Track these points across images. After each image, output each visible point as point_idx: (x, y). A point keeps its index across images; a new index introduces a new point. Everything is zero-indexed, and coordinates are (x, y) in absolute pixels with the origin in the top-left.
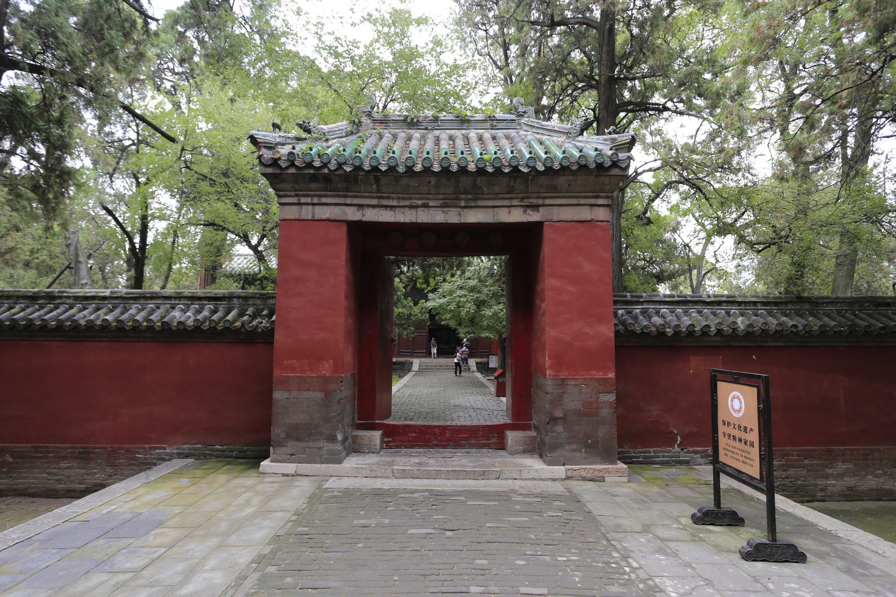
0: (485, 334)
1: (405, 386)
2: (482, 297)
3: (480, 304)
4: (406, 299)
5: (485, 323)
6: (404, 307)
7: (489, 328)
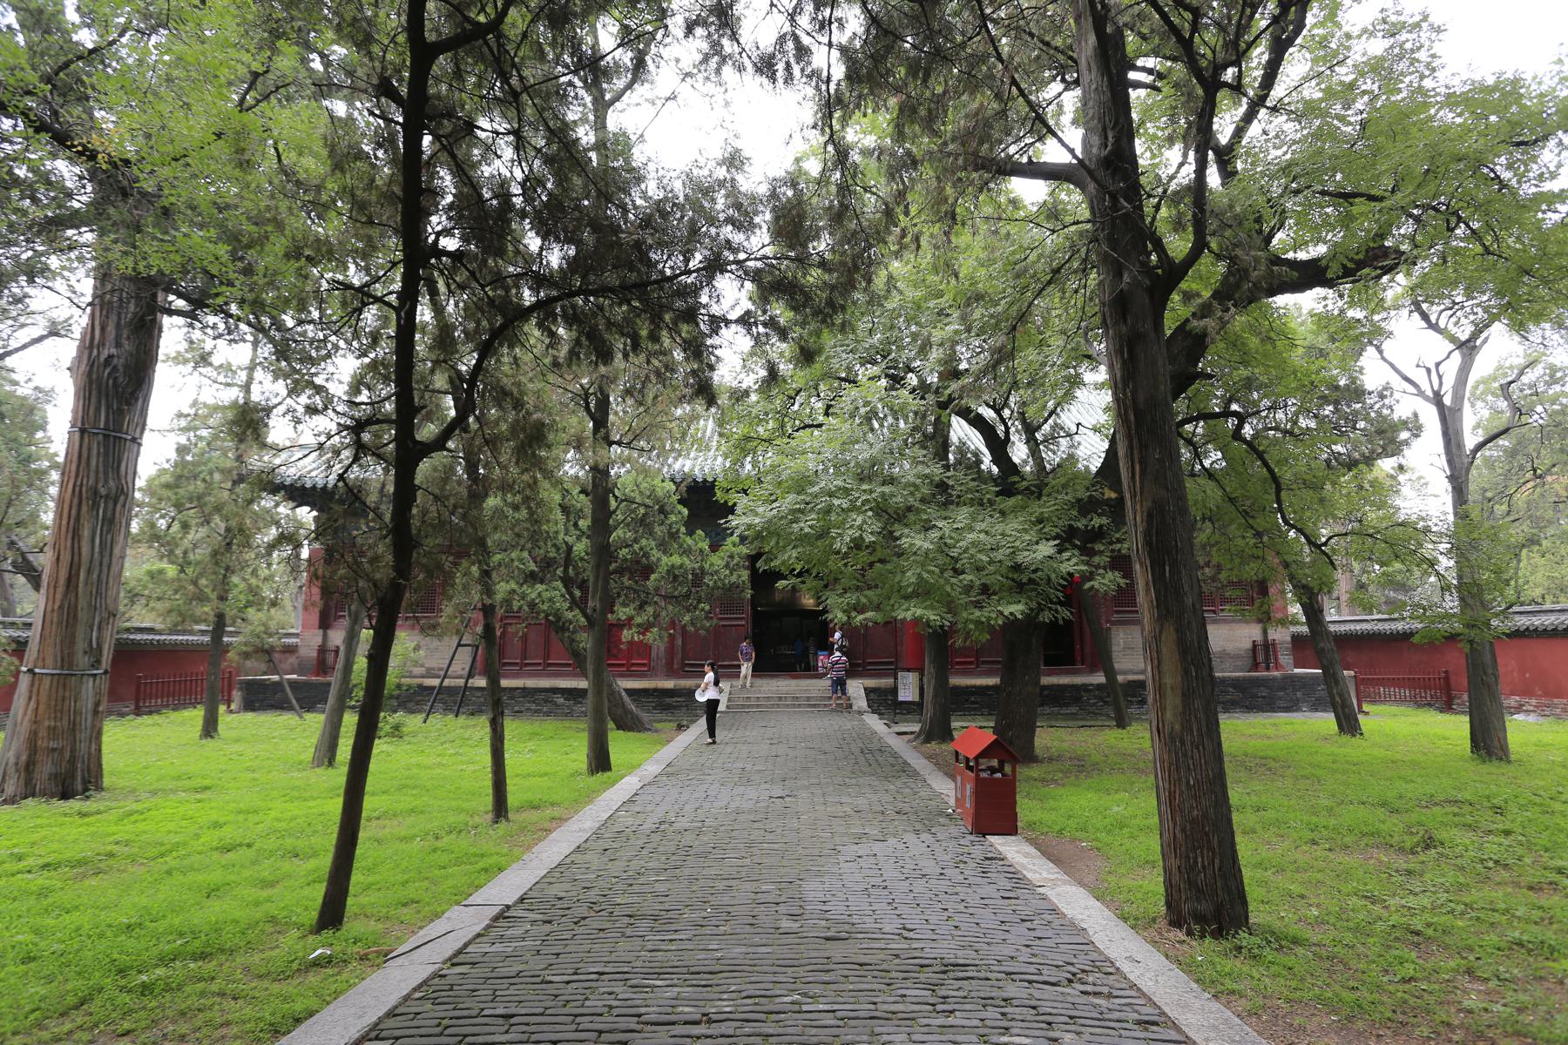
0: (910, 612)
1: (670, 771)
2: (899, 499)
3: (892, 516)
4: (690, 533)
5: (911, 577)
6: (687, 552)
7: (922, 592)
